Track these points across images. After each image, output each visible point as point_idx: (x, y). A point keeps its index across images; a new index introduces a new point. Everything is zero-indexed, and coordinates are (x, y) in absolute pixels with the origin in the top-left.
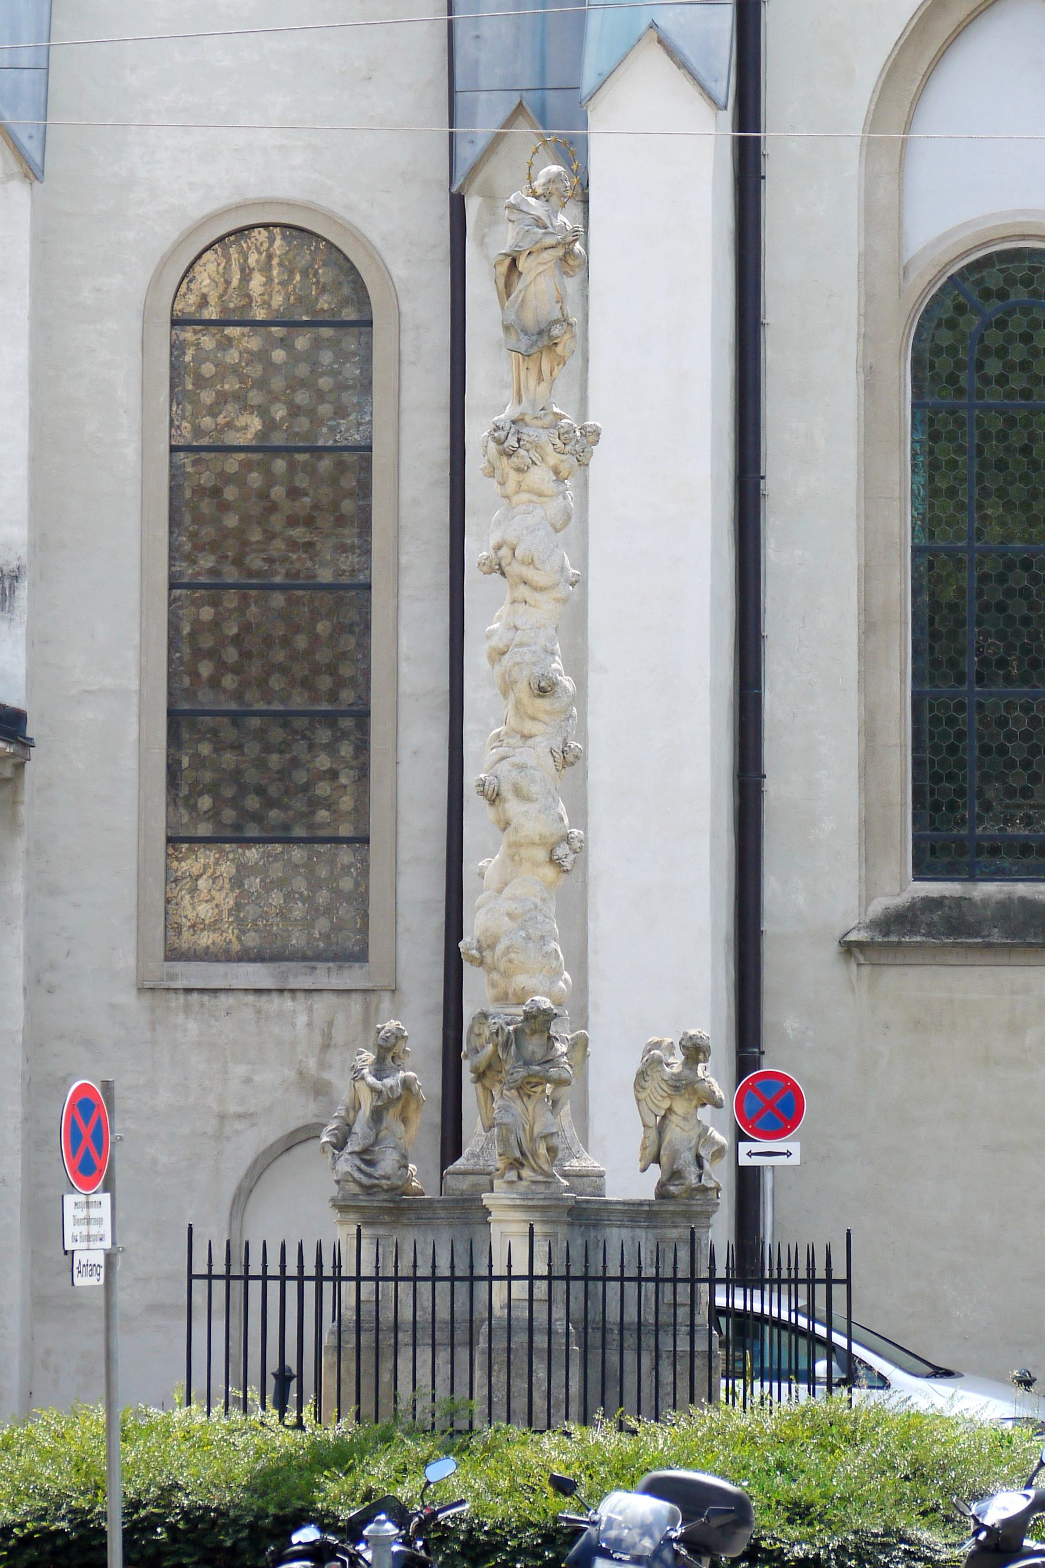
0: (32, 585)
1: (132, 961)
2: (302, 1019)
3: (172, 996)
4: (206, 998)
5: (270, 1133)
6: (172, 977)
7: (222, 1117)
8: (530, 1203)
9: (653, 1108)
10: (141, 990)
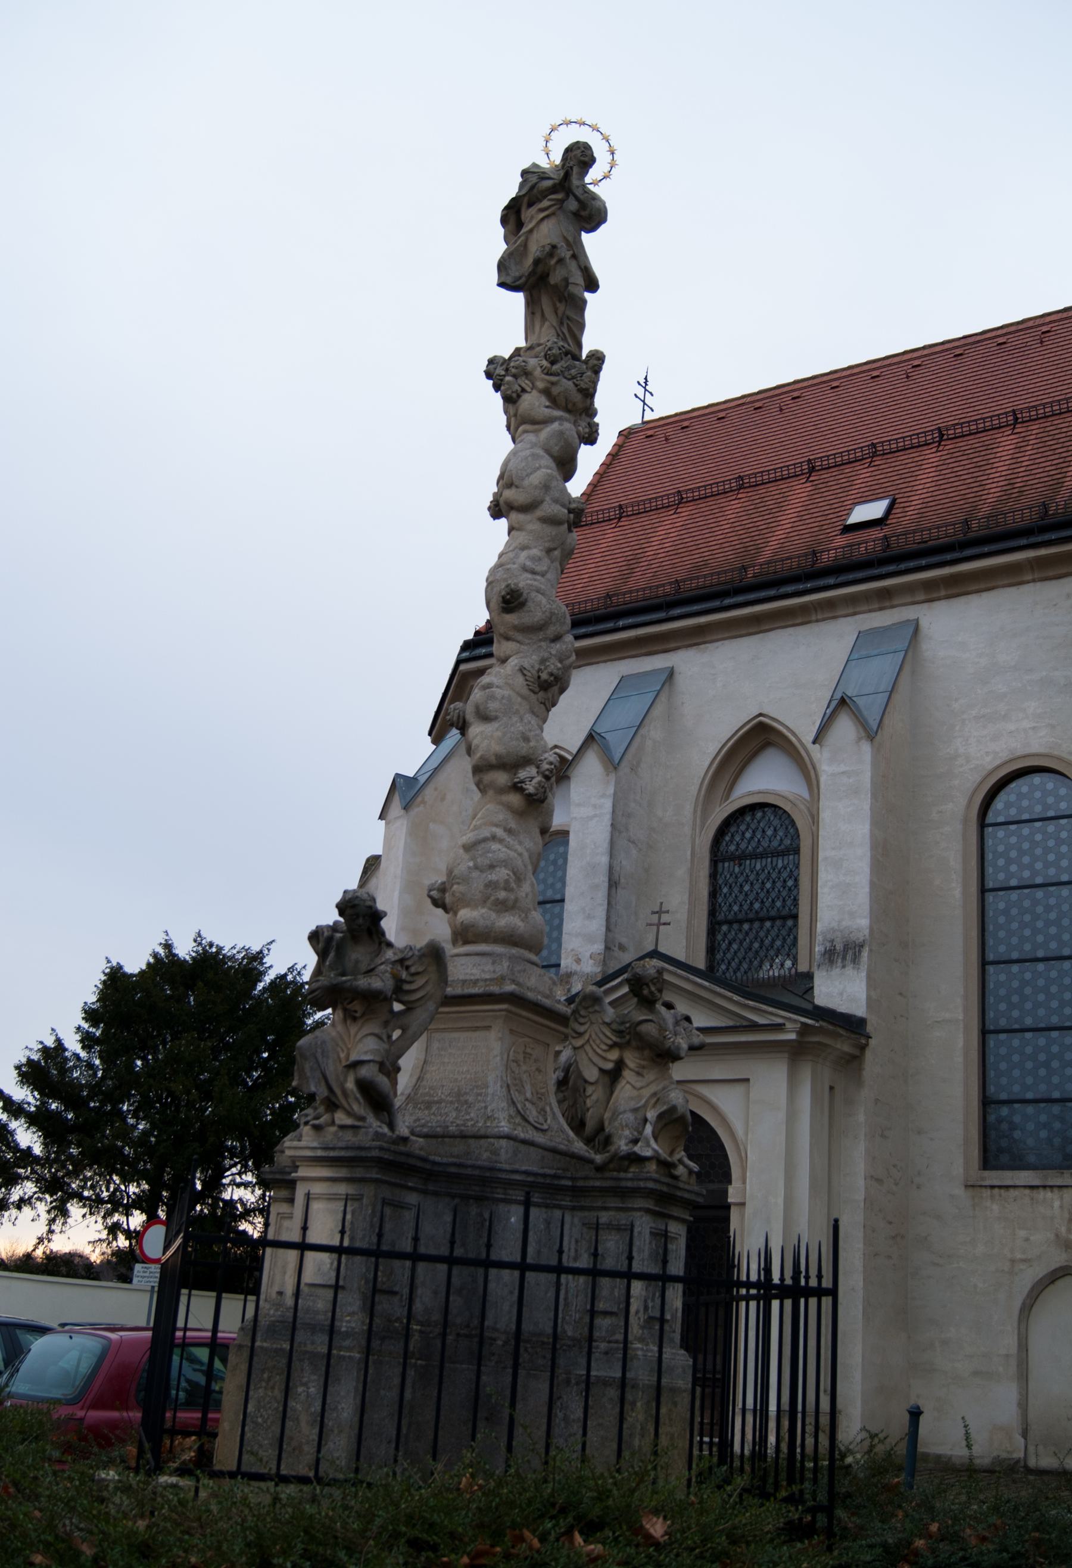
0: (871, 950)
1: (961, 1170)
2: (1057, 1204)
3: (984, 1190)
4: (1002, 1191)
5: (1039, 1271)
6: (983, 1179)
7: (1013, 1261)
8: (332, 1154)
9: (596, 1059)
10: (966, 1186)
